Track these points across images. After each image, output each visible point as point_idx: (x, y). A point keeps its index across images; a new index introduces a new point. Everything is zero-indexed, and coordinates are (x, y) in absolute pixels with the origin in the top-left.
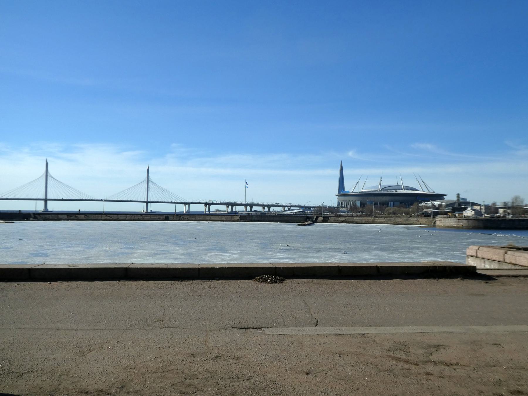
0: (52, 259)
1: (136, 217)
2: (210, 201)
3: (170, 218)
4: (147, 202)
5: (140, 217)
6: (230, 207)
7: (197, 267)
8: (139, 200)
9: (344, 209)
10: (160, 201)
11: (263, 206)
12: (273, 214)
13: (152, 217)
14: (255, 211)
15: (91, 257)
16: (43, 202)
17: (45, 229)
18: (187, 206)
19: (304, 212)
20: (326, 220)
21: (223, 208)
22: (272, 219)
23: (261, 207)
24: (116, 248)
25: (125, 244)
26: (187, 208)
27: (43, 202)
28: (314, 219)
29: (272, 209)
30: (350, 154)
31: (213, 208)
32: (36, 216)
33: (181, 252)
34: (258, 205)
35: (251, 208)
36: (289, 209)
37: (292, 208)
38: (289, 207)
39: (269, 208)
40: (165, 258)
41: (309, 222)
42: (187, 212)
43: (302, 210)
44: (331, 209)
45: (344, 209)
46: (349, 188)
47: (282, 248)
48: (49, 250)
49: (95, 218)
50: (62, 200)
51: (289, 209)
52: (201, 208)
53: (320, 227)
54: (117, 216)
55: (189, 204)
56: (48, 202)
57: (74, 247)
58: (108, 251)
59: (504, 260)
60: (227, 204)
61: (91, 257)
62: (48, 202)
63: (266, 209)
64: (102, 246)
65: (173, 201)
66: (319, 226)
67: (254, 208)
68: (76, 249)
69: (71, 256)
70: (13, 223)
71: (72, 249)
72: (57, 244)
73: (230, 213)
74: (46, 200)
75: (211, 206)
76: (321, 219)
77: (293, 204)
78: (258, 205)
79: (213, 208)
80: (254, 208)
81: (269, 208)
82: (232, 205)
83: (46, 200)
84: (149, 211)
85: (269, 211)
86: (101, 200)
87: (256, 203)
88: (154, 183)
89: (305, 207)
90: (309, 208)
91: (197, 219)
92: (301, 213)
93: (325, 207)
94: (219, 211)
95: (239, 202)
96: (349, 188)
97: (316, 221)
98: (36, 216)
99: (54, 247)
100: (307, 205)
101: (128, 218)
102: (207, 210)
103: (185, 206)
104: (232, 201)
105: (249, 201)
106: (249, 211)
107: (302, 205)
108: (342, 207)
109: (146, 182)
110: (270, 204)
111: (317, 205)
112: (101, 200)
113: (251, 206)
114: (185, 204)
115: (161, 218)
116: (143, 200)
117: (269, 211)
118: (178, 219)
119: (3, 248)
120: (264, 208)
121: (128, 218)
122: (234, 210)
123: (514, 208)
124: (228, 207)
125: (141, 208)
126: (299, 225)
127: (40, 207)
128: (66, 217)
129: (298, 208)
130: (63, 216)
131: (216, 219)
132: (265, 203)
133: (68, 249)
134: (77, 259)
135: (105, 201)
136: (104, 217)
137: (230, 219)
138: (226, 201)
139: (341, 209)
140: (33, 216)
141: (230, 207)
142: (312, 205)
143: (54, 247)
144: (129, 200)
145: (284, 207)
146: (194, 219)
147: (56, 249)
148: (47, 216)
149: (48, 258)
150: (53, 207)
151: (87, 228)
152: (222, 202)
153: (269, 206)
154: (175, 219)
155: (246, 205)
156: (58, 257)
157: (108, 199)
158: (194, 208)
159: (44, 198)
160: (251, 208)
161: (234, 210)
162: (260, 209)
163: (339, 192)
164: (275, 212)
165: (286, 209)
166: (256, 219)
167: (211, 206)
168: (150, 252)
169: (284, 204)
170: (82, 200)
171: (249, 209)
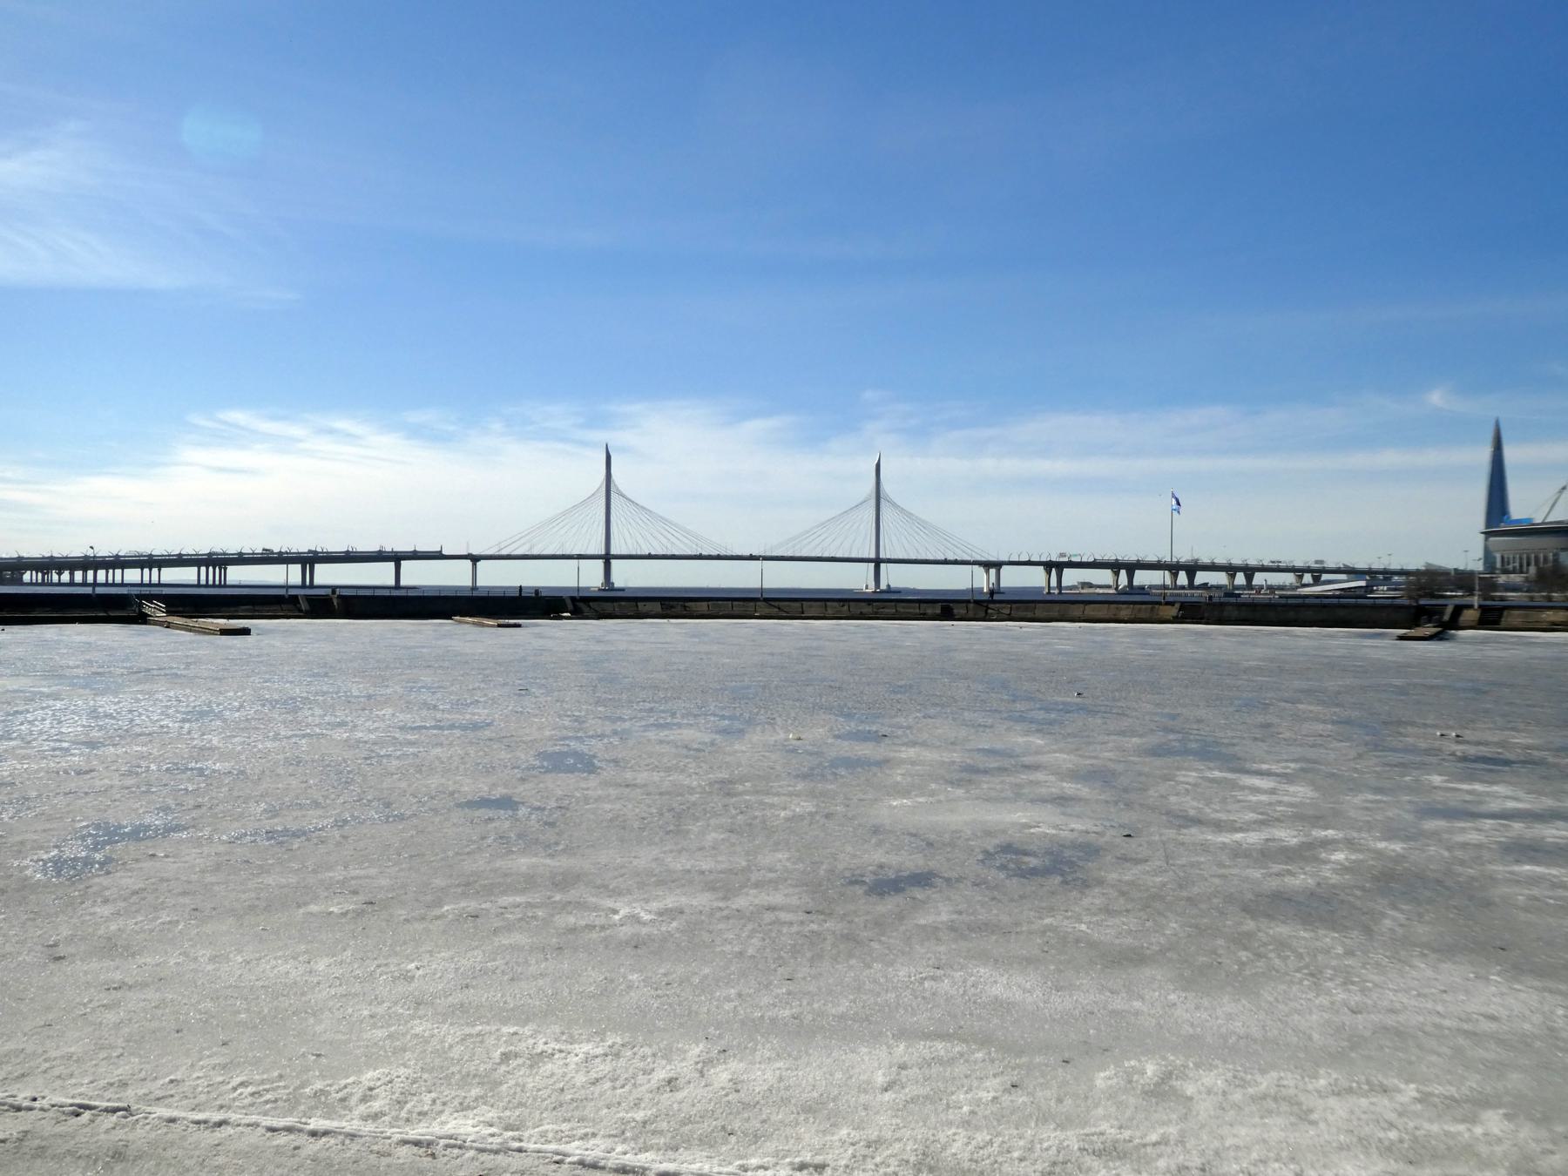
0: (606, 784)
1: (855, 609)
2: (1062, 555)
3: (304, 606)
4: (878, 562)
5: (867, 609)
6: (1123, 573)
7: (469, 594)
8: (853, 555)
9: (1516, 578)
10: (913, 557)
11: (1231, 570)
12: (1264, 597)
13: (901, 608)
14: (1205, 586)
15: (742, 780)
16: (600, 563)
17: (599, 648)
18: (993, 571)
19: (1369, 589)
20: (578, 614)
21: (1104, 577)
22: (1291, 615)
23: (1108, 572)
24: (817, 732)
25: (849, 716)
26: (993, 579)
27: (600, 563)
28: (1446, 618)
29: (1259, 579)
30: (1436, 398)
31: (1071, 577)
32: (581, 605)
33: (1065, 759)
34: (1213, 567)
35: (1191, 577)
36: (1317, 581)
37: (1325, 577)
38: (1317, 573)
39: (1249, 578)
40: (1017, 795)
41: (1429, 630)
42: (992, 592)
43: (1363, 583)
44: (1463, 580)
45: (1516, 578)
46: (1525, 505)
47: (1459, 749)
48: (602, 736)
49: (736, 611)
50: (650, 557)
51: (1317, 581)
52: (1035, 579)
53: (1471, 644)
54: (797, 604)
55: (998, 565)
56: (613, 562)
57: (680, 726)
58: (794, 751)
59: (474, 565)
60: (1115, 566)
61: (742, 780)
62: (613, 562)
63: (1240, 579)
64: (772, 722)
65: (951, 557)
66: (1466, 641)
67: (1259, 579)
68: (688, 734)
69: (668, 770)
70: (519, 626)
71: (673, 734)
72: (627, 713)
73: (1123, 592)
74: (607, 558)
75: (1066, 571)
76: (1470, 615)
77: (1330, 564)
78: (1213, 567)
79: (1071, 577)
80: (1201, 577)
81: (1249, 578)
82: (1131, 567)
83: (607, 558)
84: (883, 586)
85: (1249, 586)
86: (752, 558)
87: (1206, 560)
88: (894, 505)
89: (1370, 572)
90: (1388, 574)
91: (1038, 613)
92: (1362, 592)
93: (1445, 573)
94: (1090, 585)
95: (1152, 558)
96: (1525, 505)
97: (1454, 623)
98: (581, 605)
99: (619, 726)
100: (1377, 565)
101: (830, 611)
102: (1054, 583)
103: (987, 572)
104: (1131, 556)
105: (1184, 556)
106: (1183, 588)
107: (1361, 565)
108: (1505, 572)
109: (873, 502)
110: (1252, 562)
111: (1412, 567)
112: (752, 558)
113: (1192, 569)
114: (987, 565)
115: (929, 611)
116: (866, 556)
117: (1249, 586)
118: (982, 614)
119: (464, 728)
120: (1233, 577)
121: (830, 611)
122: (1136, 583)
123: (380, 552)
124: (1117, 574)
125: (858, 579)
126: (1401, 638)
127: (590, 577)
128: (657, 607)
129: (1343, 577)
130: (649, 606)
131: (1100, 615)
132: (1237, 561)
133: (663, 734)
134: (691, 790)
135: (766, 558)
136: (763, 608)
137: (1110, 615)
138: (1110, 556)
139: (1502, 579)
140: (570, 607)
141: (1123, 573)
142: (1395, 566)
143: (619, 726)
144: (826, 555)
145: (1299, 572)
146: (1030, 615)
147: (623, 736)
148: (608, 607)
149: (593, 781)
150: (628, 576)
151: (715, 648)
152: (1098, 557)
153: (1249, 571)
154: (971, 614)
155: (1174, 568)
156: (629, 775)
157: (768, 554)
158: (1012, 579)
159: (873, 555)
160: (1191, 577)
161: (1136, 583)
162: (1220, 578)
163: (1489, 523)
164: (1271, 588)
165: (1308, 578)
166: (1235, 614)
167: (1066, 571)
168: (946, 757)
169: (1299, 564)
170: (700, 557)
171: (1183, 578)
